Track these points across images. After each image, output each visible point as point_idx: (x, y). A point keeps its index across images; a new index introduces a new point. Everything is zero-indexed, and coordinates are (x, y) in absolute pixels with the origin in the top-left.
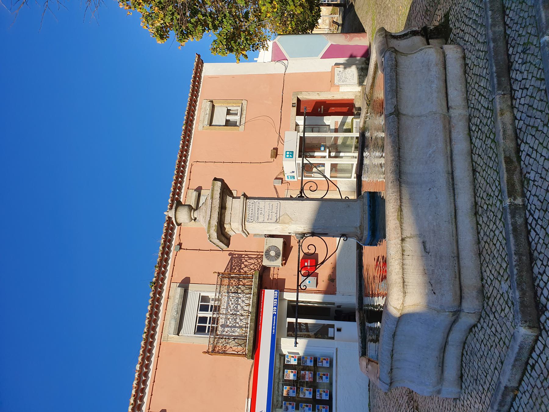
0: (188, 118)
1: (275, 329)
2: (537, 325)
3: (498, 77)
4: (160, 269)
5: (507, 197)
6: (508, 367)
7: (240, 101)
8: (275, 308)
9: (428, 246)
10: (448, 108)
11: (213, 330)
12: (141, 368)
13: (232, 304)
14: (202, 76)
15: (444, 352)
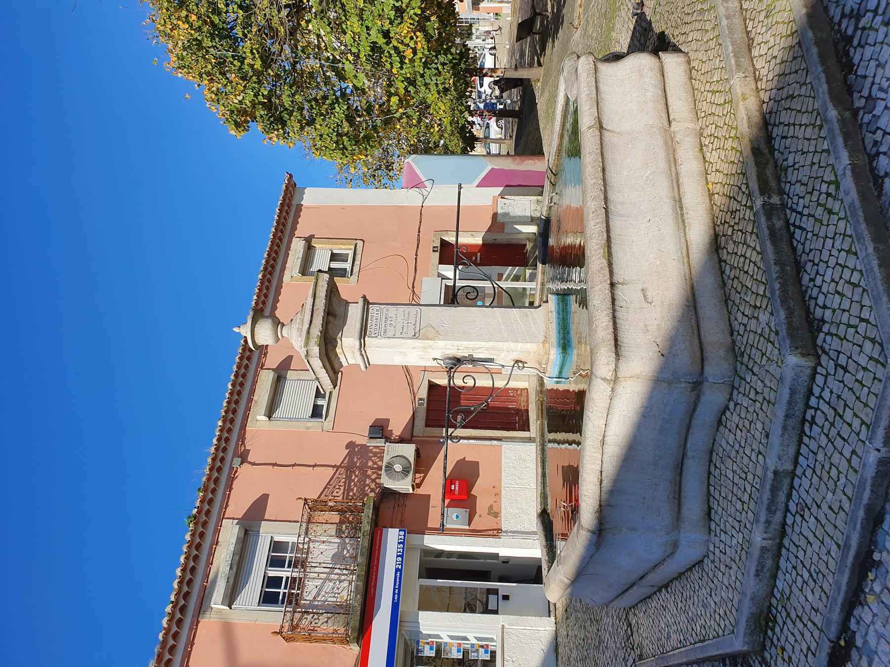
1: (399, 594)
2: (814, 351)
3: (736, 56)
6: (775, 439)
7: (354, 242)
8: (400, 559)
10: (670, 122)
11: (293, 600)
15: (681, 474)
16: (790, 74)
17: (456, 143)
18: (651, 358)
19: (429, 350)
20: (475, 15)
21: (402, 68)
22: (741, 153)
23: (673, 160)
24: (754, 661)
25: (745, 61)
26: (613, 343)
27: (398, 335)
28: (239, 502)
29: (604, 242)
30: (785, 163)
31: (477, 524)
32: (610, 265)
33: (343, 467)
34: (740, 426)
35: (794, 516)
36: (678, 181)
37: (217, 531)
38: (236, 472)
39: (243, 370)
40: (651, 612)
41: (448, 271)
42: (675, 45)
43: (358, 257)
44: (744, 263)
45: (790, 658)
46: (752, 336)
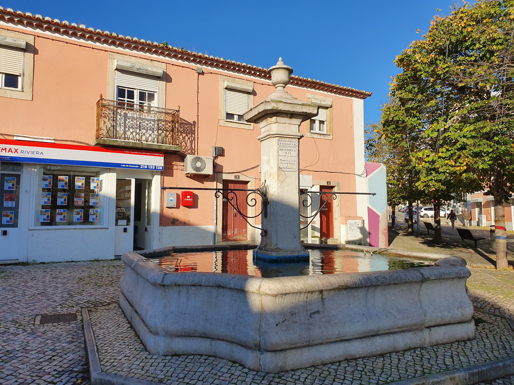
0: (317, 83)
1: (126, 167)
3: (479, 373)
4: (180, 53)
7: (331, 134)
8: (146, 167)
9: (316, 316)
10: (429, 327)
11: (121, 105)
12: (82, 30)
13: (147, 124)
14: (353, 98)
15: (201, 337)
27: (280, 158)
34: (232, 376)
43: (322, 137)
44: (340, 379)
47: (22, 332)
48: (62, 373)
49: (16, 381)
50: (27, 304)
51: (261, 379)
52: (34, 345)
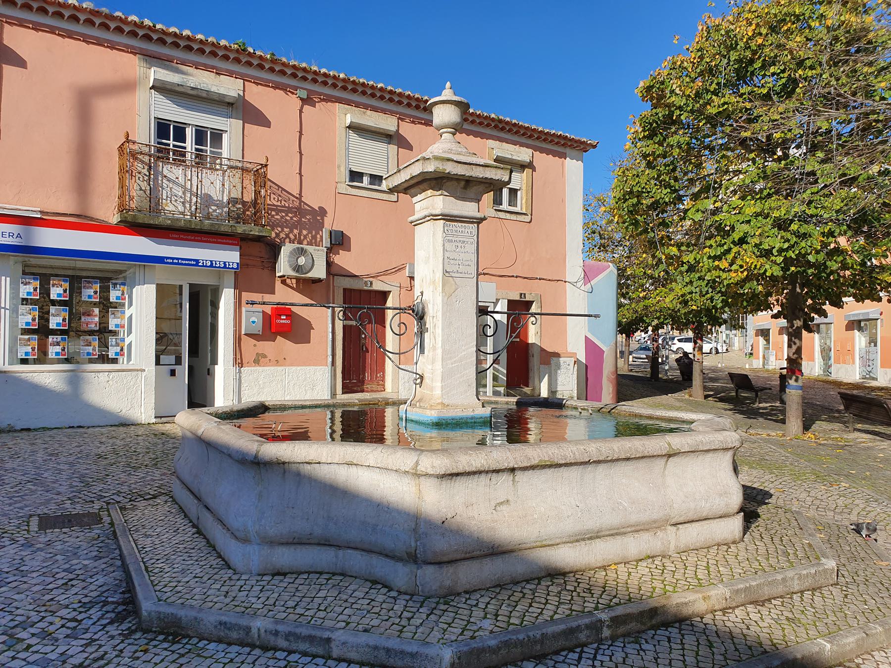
5: (610, 616)
6: (363, 639)
7: (529, 213)
8: (209, 264)
9: (503, 507)
10: (675, 525)
11: (162, 154)
15: (319, 544)
16: (734, 643)
17: (629, 315)
18: (439, 511)
19: (431, 287)
20: (751, 332)
21: (710, 257)
22: (651, 597)
23: (638, 529)
24: (130, 622)
25: (741, 598)
26: (455, 471)
27: (447, 254)
28: (261, 97)
29: (556, 461)
30: (643, 642)
31: (247, 343)
32: (533, 468)
33: (300, 204)
34: (372, 603)
35: (285, 659)
36: (617, 534)
37: (230, 74)
38: (293, 93)
39: (396, 99)
40: (170, 518)
41: (502, 306)
42: (749, 528)
43: (513, 217)
44: (539, 603)
45: (138, 658)
46: (468, 612)
47: (9, 543)
48: (88, 606)
49: (12, 620)
50: (10, 498)
51: (418, 606)
52: (35, 562)
